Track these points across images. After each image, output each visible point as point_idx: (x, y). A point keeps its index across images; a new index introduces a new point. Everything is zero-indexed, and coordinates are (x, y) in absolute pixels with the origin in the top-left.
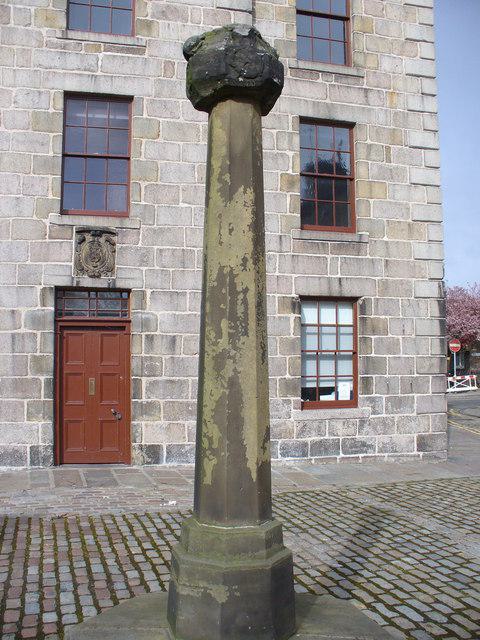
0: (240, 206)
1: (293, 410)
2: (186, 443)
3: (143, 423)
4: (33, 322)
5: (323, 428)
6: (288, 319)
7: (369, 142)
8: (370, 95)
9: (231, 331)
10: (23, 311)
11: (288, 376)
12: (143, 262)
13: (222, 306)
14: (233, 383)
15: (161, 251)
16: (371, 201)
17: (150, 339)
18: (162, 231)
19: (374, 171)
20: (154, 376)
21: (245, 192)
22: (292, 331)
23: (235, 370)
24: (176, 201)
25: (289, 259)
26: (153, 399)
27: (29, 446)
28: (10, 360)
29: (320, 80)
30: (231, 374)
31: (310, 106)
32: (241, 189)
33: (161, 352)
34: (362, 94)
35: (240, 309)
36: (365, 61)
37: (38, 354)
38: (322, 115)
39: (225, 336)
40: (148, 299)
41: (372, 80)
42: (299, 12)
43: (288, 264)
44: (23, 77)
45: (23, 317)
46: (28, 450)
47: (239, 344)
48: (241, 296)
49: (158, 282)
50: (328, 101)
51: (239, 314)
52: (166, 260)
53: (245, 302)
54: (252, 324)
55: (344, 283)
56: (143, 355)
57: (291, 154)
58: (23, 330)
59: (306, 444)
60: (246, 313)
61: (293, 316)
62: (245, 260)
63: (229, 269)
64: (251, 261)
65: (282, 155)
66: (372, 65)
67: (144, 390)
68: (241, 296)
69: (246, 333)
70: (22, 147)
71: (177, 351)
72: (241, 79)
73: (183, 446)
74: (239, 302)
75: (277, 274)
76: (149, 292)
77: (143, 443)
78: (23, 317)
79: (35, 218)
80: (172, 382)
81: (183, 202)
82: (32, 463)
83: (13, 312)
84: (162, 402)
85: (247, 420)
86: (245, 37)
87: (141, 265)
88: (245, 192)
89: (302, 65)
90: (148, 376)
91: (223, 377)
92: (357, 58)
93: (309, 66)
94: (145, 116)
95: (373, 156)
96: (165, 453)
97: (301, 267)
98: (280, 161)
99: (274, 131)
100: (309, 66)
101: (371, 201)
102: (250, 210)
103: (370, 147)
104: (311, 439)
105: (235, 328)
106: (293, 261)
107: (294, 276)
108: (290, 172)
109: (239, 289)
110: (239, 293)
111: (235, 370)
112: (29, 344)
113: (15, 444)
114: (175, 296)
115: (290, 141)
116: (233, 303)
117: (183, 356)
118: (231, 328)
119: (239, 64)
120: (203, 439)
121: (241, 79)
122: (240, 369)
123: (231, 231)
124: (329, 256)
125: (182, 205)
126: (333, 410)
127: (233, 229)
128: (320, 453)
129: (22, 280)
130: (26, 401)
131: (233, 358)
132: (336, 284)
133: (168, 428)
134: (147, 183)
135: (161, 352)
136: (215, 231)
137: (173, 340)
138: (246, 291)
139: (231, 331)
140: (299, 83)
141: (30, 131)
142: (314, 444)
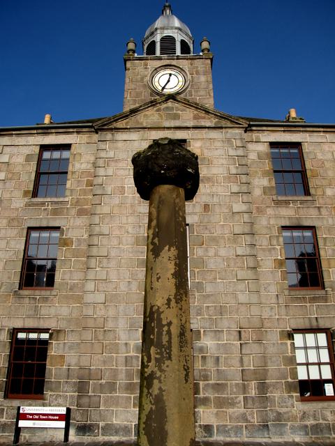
0: (165, 260)
1: (295, 403)
2: (228, 424)
3: (201, 410)
5: (317, 416)
6: (286, 344)
7: (324, 236)
8: (322, 210)
9: (157, 356)
10: (132, 343)
11: (290, 380)
12: (198, 314)
13: (152, 337)
14: (159, 400)
15: (208, 307)
16: (330, 270)
17: (204, 358)
18: (208, 296)
19: (330, 252)
20: (207, 380)
21: (169, 250)
22: (289, 351)
23: (160, 389)
24: (215, 279)
25: (283, 307)
26: (207, 395)
29: (291, 205)
31: (287, 219)
32: (167, 248)
33: (210, 365)
34: (316, 209)
35: (165, 339)
36: (316, 192)
38: (294, 223)
39: (153, 361)
40: (202, 335)
41: (321, 201)
42: (275, 171)
43: (283, 311)
44: (131, 220)
45: (132, 347)
46: (133, 426)
47: (164, 367)
48: (165, 329)
49: (207, 325)
50: (297, 216)
51: (164, 343)
52: (211, 313)
53: (169, 332)
54: (175, 350)
55: (319, 320)
56: (200, 368)
57: (278, 247)
58: (132, 354)
59: (306, 426)
60: (170, 342)
61: (289, 342)
62: (169, 300)
63: (157, 308)
64: (173, 301)
65: (274, 249)
66: (320, 193)
67: (201, 388)
68: (165, 329)
69: (170, 358)
71: (220, 365)
72: (162, 172)
73: (226, 426)
74: (164, 333)
75: (277, 317)
76: (202, 331)
77: (202, 423)
78: (132, 347)
80: (218, 384)
81: (219, 279)
83: (126, 344)
84: (212, 396)
85: (170, 433)
86: (166, 144)
87: (197, 315)
88: (169, 250)
89: (280, 198)
90: (204, 381)
91: (151, 395)
92: (312, 191)
93: (284, 198)
94: (195, 234)
95: (328, 244)
96: (215, 431)
97: (291, 312)
98: (273, 252)
99: (268, 236)
100: (284, 198)
101: (330, 270)
102: (173, 263)
103: (325, 239)
104: (309, 423)
105: (161, 353)
106: (286, 309)
107: (288, 318)
108: (279, 258)
109: (164, 322)
110: (164, 326)
111: (160, 389)
113: (126, 423)
114: (218, 333)
115: (278, 241)
116: (160, 334)
117: (223, 368)
118: (157, 353)
119: (161, 162)
121: (162, 172)
122: (163, 388)
123: (158, 279)
124: (308, 305)
125: (218, 281)
127: (160, 278)
128: (317, 433)
129: (131, 326)
130: (132, 396)
131: (159, 378)
132: (314, 321)
133: (217, 414)
134: (198, 270)
135: (210, 365)
136: (149, 279)
137: (218, 359)
138: (170, 324)
139: (157, 356)
140: (279, 209)
142: (313, 426)
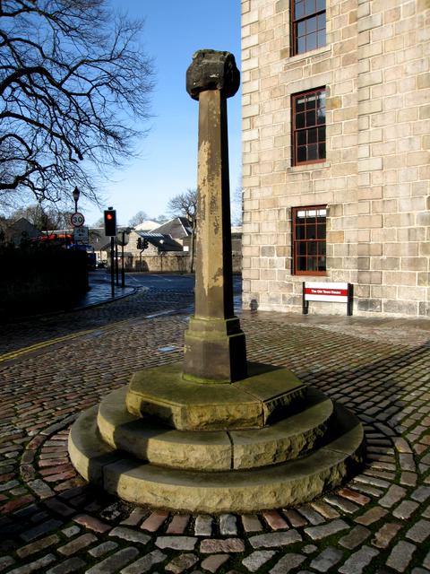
4: (422, 220)
10: (416, 213)
27: (418, 302)
28: (407, 246)
30: (151, 250)
37: (426, 242)
45: (415, 217)
53: (204, 202)
58: (416, 226)
60: (204, 208)
70: (411, 103)
78: (415, 217)
79: (422, 150)
82: (420, 313)
83: (409, 214)
112: (419, 233)
113: (409, 300)
120: (258, 487)
126: (231, 200)
130: (417, 272)
141: (417, 90)
